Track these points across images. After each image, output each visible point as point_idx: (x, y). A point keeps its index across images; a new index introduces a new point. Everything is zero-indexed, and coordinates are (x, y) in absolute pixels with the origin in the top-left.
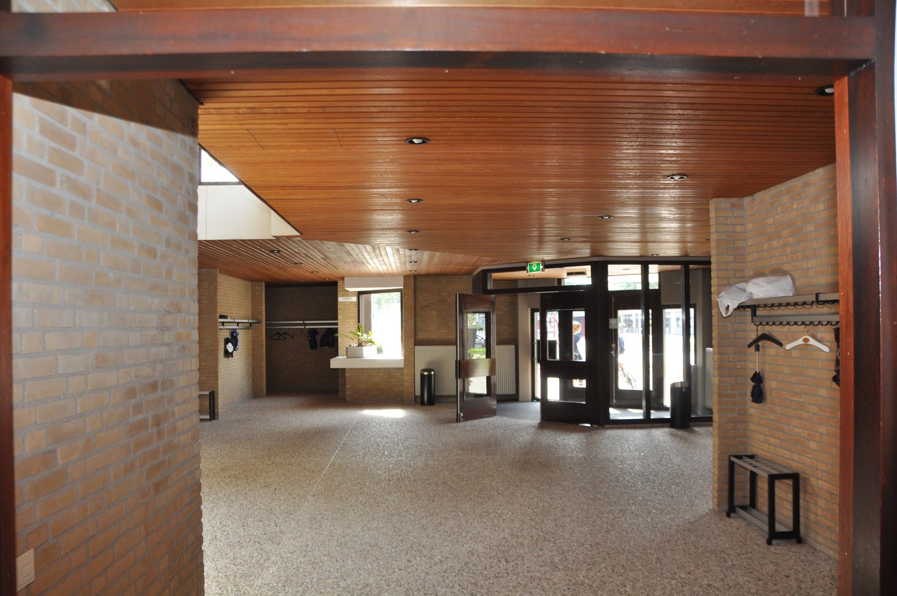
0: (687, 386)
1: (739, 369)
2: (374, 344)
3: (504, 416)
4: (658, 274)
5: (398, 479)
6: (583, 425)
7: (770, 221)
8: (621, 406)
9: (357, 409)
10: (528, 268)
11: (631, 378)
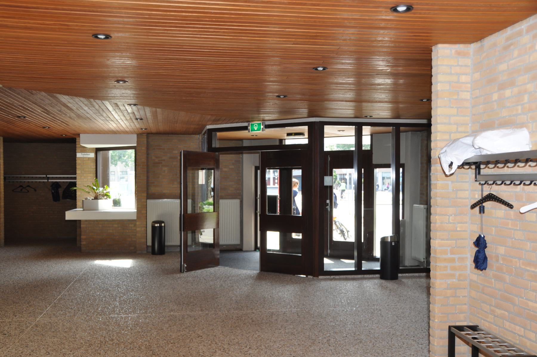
0: (396, 240)
1: (459, 231)
2: (109, 198)
3: (227, 266)
4: (370, 136)
5: (101, 342)
6: (299, 276)
7: (503, 67)
8: (335, 257)
9: (90, 259)
10: (250, 128)
11: (345, 230)
